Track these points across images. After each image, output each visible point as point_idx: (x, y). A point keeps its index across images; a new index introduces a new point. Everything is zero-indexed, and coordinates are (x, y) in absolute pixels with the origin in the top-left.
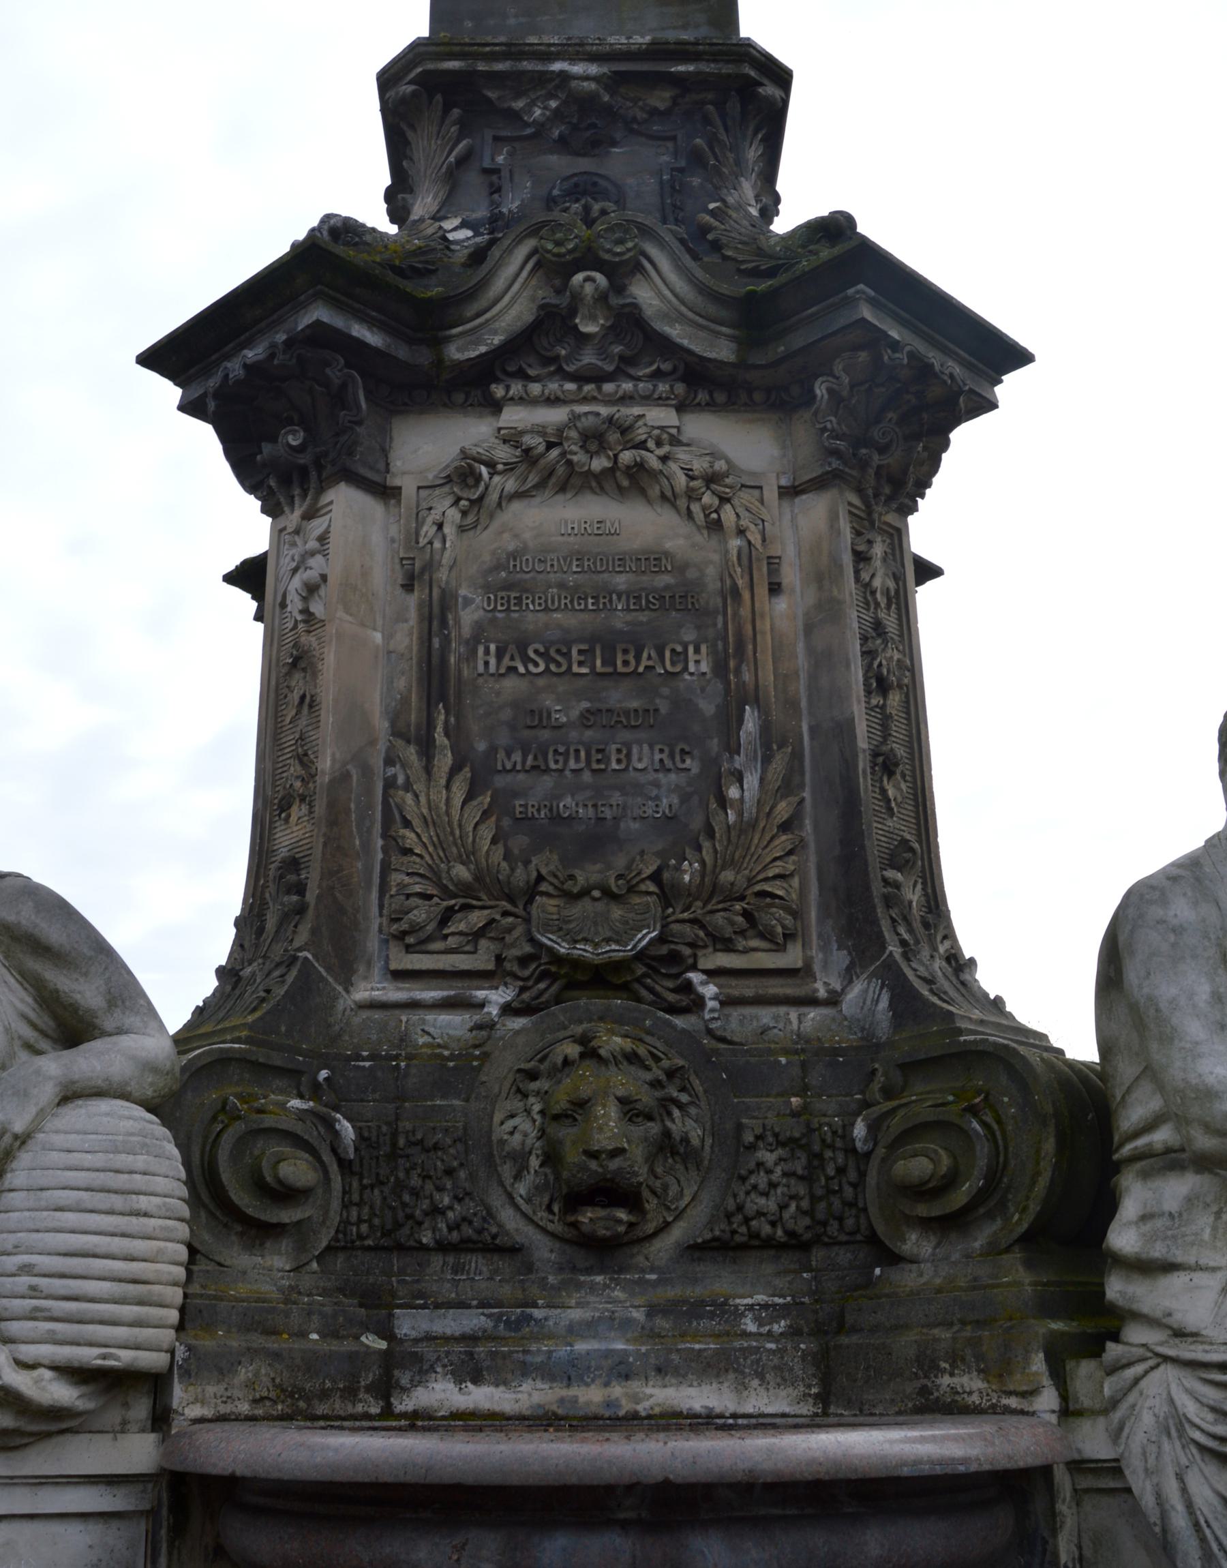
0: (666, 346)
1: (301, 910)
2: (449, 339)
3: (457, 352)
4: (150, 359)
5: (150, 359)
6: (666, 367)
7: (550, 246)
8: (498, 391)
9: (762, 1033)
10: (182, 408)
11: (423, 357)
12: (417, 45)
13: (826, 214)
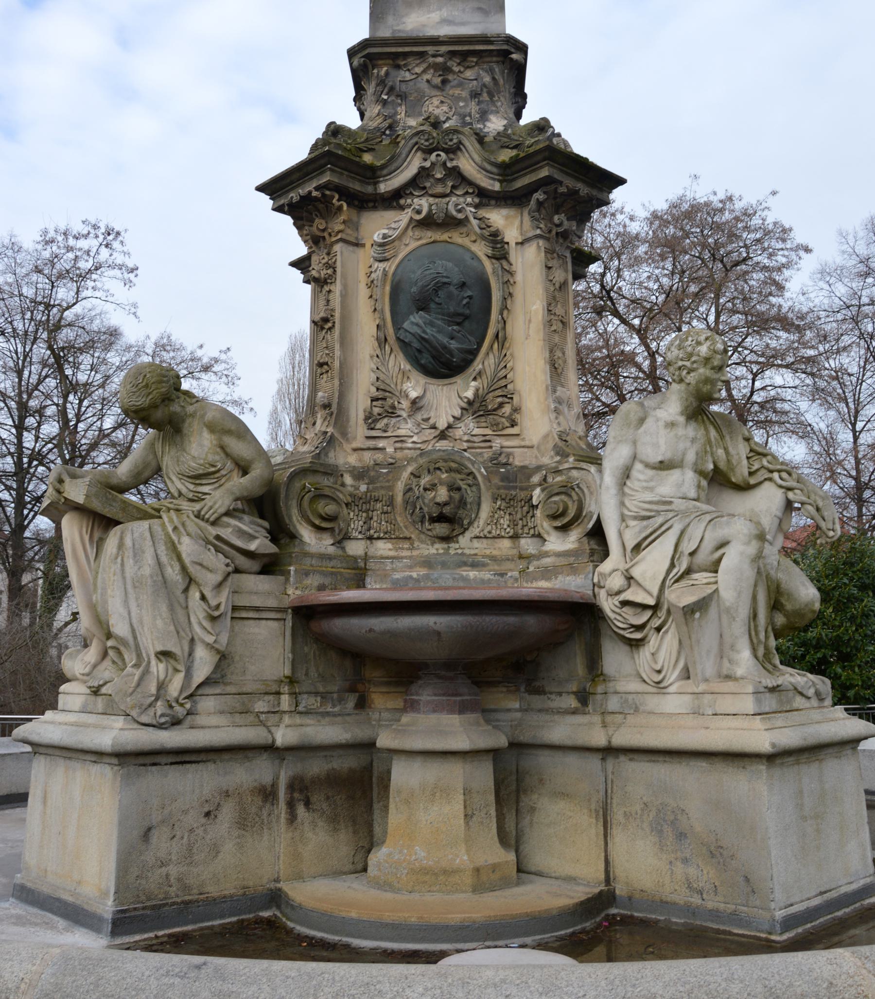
0: (470, 183)
1: (332, 414)
2: (379, 182)
3: (384, 187)
4: (261, 188)
5: (261, 188)
6: (471, 191)
7: (423, 141)
8: (402, 202)
9: (583, 366)
10: (274, 209)
11: (370, 189)
12: (366, 40)
13: (537, 119)
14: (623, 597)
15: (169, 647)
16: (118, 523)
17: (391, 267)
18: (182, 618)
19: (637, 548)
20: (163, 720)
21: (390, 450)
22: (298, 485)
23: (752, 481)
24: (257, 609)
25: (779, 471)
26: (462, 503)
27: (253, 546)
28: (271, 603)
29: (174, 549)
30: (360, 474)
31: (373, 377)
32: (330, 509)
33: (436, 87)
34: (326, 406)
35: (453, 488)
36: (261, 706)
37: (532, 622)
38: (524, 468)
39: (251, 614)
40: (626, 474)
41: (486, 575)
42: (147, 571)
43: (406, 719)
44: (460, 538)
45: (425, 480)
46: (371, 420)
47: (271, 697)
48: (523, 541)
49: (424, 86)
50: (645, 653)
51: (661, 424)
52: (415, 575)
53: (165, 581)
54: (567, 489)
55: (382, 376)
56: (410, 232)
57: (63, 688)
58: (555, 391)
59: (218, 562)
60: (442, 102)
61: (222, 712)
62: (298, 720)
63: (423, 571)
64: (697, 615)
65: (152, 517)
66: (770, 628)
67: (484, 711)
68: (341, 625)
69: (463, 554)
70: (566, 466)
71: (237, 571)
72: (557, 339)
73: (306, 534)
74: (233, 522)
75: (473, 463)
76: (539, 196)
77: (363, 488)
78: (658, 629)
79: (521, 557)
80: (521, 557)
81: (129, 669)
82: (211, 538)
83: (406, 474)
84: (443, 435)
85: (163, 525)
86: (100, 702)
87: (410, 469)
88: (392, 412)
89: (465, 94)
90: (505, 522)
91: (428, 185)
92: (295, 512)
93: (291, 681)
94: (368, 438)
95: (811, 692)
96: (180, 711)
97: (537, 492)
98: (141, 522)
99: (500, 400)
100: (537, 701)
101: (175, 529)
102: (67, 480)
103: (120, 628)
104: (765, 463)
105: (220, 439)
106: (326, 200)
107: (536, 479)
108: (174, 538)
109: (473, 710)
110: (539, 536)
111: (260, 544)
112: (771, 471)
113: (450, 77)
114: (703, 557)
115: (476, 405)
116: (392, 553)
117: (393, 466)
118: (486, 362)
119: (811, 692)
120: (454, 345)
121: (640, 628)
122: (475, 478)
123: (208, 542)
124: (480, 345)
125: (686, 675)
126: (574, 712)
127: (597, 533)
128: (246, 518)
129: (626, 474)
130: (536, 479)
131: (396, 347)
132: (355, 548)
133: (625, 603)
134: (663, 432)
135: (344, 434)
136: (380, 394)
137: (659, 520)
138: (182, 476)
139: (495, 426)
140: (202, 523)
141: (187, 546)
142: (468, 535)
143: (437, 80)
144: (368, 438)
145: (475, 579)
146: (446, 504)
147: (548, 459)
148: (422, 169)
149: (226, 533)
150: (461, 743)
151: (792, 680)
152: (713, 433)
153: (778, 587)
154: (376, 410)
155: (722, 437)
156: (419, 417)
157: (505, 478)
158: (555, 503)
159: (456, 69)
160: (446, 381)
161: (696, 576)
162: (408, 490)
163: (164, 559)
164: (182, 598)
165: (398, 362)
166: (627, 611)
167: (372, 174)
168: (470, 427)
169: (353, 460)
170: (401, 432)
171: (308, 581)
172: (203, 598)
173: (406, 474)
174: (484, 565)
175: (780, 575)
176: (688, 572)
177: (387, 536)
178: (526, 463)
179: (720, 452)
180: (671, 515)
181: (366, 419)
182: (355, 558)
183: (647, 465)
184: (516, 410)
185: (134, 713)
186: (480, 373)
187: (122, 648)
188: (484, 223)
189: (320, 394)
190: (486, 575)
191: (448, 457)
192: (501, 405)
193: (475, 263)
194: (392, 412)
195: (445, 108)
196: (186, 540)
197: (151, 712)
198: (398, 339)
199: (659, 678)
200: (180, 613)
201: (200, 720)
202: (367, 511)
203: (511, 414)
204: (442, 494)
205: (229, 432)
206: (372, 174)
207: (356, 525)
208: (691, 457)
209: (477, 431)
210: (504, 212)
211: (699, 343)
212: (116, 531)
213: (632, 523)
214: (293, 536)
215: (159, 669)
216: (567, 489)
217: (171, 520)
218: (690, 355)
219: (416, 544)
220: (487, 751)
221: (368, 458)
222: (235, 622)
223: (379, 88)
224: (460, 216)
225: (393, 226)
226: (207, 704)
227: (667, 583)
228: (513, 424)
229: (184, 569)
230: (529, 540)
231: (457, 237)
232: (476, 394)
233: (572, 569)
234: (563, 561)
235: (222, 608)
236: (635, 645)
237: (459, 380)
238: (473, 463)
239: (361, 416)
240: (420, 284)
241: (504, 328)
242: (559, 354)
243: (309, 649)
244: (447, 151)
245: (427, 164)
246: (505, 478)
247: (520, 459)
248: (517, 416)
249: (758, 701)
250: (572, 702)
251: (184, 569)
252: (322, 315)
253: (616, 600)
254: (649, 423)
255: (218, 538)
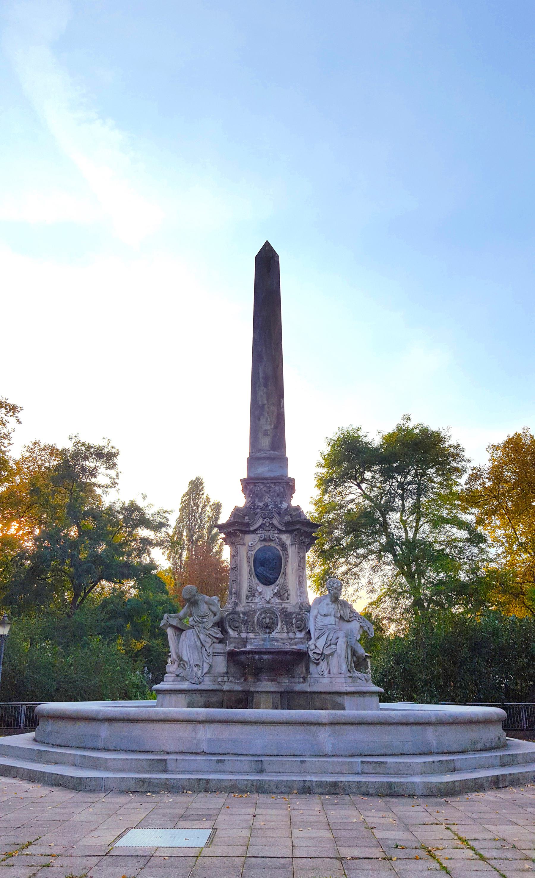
0: (276, 527)
3: (251, 529)
14: (314, 651)
15: (198, 663)
16: (184, 630)
17: (254, 553)
18: (201, 656)
19: (318, 638)
20: (197, 682)
21: (253, 606)
22: (228, 617)
23: (351, 620)
24: (218, 653)
25: (358, 617)
26: (273, 623)
27: (217, 636)
28: (222, 651)
29: (198, 636)
30: (244, 614)
31: (249, 584)
32: (237, 625)
33: (267, 492)
34: (235, 593)
35: (270, 618)
36: (220, 680)
37: (288, 657)
38: (291, 612)
39: (217, 654)
40: (316, 617)
41: (280, 644)
42: (192, 643)
43: (258, 683)
44: (273, 633)
45: (263, 616)
46: (247, 597)
47: (222, 678)
48: (290, 634)
49: (263, 492)
50: (320, 666)
51: (325, 604)
52: (260, 643)
53: (197, 646)
54: (301, 620)
55: (251, 584)
56: (259, 542)
57: (166, 675)
58: (300, 589)
59: (209, 640)
60: (269, 498)
61: (210, 681)
62: (229, 684)
63: (263, 642)
64: (331, 657)
65: (191, 628)
66: (352, 661)
67: (278, 683)
68: (243, 658)
69: (273, 638)
70: (302, 613)
71: (214, 643)
72: (301, 574)
73: (231, 632)
74: (213, 629)
75: (276, 611)
76: (296, 533)
77: (246, 618)
78: (322, 660)
79: (289, 639)
80: (289, 639)
81: (187, 669)
82: (208, 634)
83: (257, 614)
84: (268, 602)
85: (196, 631)
86: (179, 678)
87: (259, 613)
88: (253, 595)
89: (275, 495)
90: (285, 628)
91: (264, 527)
92: (227, 625)
93: (227, 673)
94: (247, 603)
95: (363, 679)
96: (201, 680)
97: (294, 620)
98: (190, 630)
99: (284, 592)
100: (293, 680)
101: (199, 632)
102: (170, 618)
103: (185, 658)
104: (354, 615)
105: (209, 606)
106: (235, 533)
107: (294, 616)
108: (199, 634)
109: (275, 681)
110: (294, 632)
111: (220, 635)
112: (356, 617)
113: (271, 489)
114: (333, 641)
115: (278, 593)
116: (254, 637)
117: (255, 612)
118: (280, 581)
119: (363, 679)
120: (271, 576)
121: (318, 660)
122: (277, 615)
123: (207, 635)
124: (279, 576)
125: (329, 673)
126: (303, 682)
127: (309, 632)
128: (216, 628)
129: (316, 617)
130: (294, 616)
131: (255, 576)
132: (243, 635)
133: (314, 653)
134: (325, 606)
135: (240, 602)
136: (250, 590)
137: (323, 631)
138: (198, 616)
139: (282, 599)
140: (205, 630)
141: (202, 637)
142: (275, 632)
143: (267, 491)
144: (247, 603)
145: (277, 645)
146: (269, 623)
147: (297, 610)
148: (263, 523)
149: (211, 633)
150: (272, 690)
151: (357, 675)
152: (340, 606)
153: (354, 650)
154: (249, 594)
155: (342, 607)
156: (261, 596)
157: (285, 615)
158: (298, 624)
159: (273, 487)
160: (269, 586)
161: (331, 646)
162: (258, 619)
163: (196, 640)
164: (200, 650)
165: (255, 580)
166: (315, 655)
167: (248, 525)
168: (276, 600)
169: (243, 609)
170: (257, 601)
171: (231, 645)
172: (206, 650)
173: (257, 614)
174: (279, 641)
175: (355, 647)
176: (330, 645)
177: (253, 632)
178: (292, 611)
179: (342, 612)
180: (326, 629)
181: (246, 597)
182: (244, 638)
183: (321, 615)
184: (289, 595)
185: (190, 680)
186: (279, 584)
187: (185, 664)
188: (280, 539)
189: (233, 590)
190: (280, 644)
191: (269, 609)
192: (284, 594)
193: (277, 552)
194: (253, 595)
195: (270, 500)
196: (202, 635)
197: (194, 680)
198: (256, 574)
199: (322, 673)
200: (200, 654)
201: (205, 683)
202: (247, 625)
203: (287, 596)
204: (268, 620)
205: (211, 604)
206: (248, 525)
207: (243, 629)
208: (333, 613)
209: (277, 601)
210: (286, 535)
211: (334, 583)
212: (184, 632)
213: (317, 631)
214: (227, 632)
215: (196, 669)
216: (301, 620)
217: (197, 629)
218: (332, 587)
219: (260, 634)
220: (278, 692)
221: (247, 609)
222: (214, 657)
223: (250, 493)
224: (273, 539)
225: (254, 541)
226: (206, 679)
227: (325, 648)
228: (288, 599)
229: (201, 642)
230: (292, 634)
231: (272, 544)
232: (278, 591)
233: (302, 643)
234: (300, 640)
235: (211, 653)
236: (318, 664)
237: (273, 586)
238: (276, 611)
239: (245, 597)
240: (262, 559)
241: (286, 571)
242: (301, 578)
243: (232, 664)
244: (270, 518)
245: (264, 522)
246: (285, 615)
247: (290, 609)
248: (289, 597)
249: (346, 680)
250: (301, 680)
251: (201, 642)
252: (234, 566)
253: (312, 652)
254: (322, 603)
255: (209, 634)
